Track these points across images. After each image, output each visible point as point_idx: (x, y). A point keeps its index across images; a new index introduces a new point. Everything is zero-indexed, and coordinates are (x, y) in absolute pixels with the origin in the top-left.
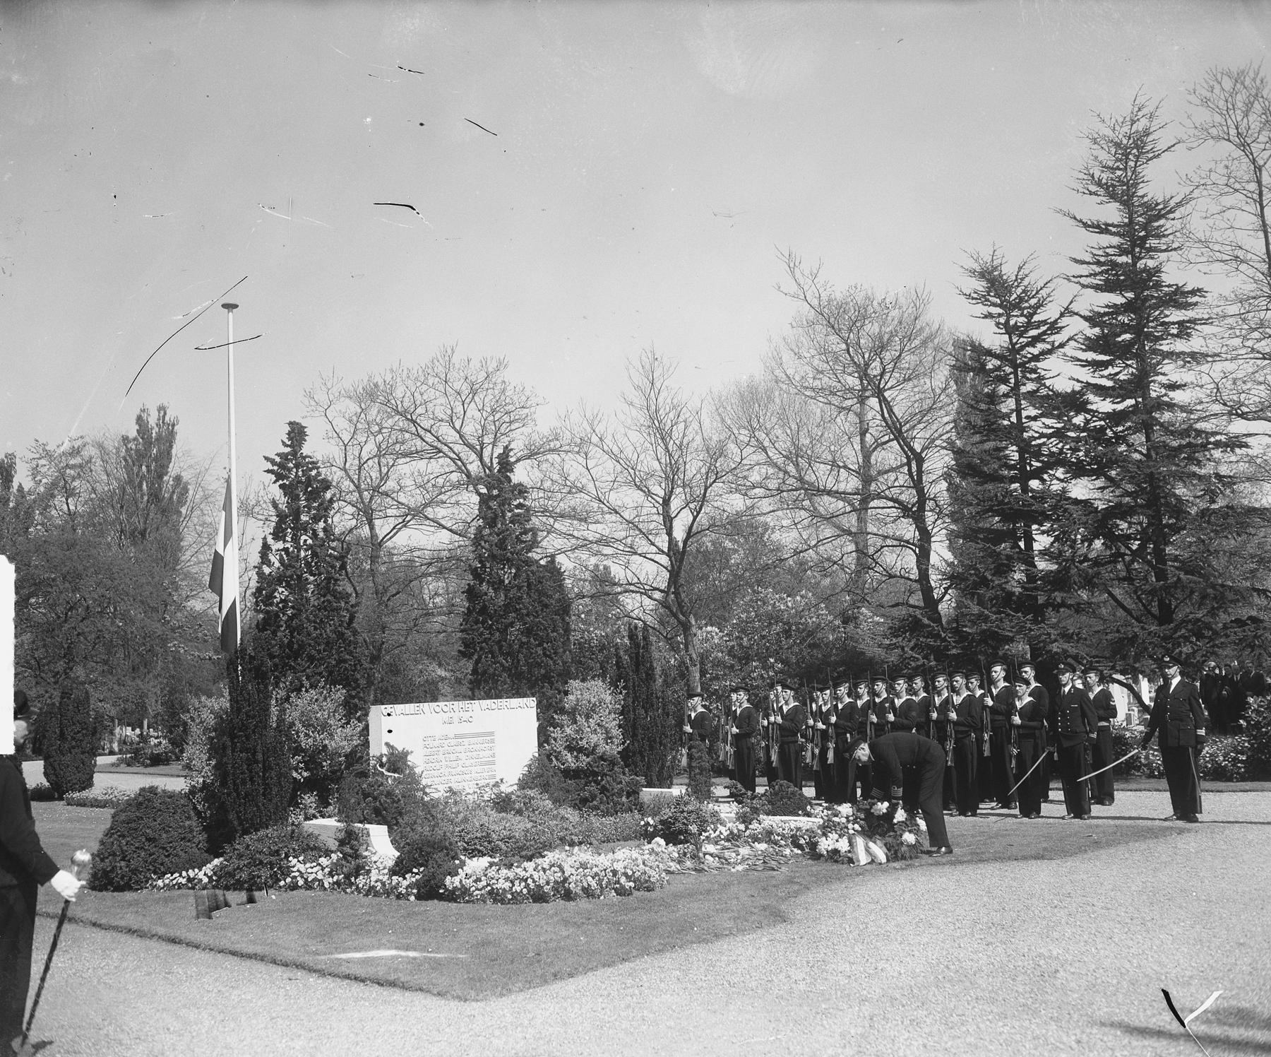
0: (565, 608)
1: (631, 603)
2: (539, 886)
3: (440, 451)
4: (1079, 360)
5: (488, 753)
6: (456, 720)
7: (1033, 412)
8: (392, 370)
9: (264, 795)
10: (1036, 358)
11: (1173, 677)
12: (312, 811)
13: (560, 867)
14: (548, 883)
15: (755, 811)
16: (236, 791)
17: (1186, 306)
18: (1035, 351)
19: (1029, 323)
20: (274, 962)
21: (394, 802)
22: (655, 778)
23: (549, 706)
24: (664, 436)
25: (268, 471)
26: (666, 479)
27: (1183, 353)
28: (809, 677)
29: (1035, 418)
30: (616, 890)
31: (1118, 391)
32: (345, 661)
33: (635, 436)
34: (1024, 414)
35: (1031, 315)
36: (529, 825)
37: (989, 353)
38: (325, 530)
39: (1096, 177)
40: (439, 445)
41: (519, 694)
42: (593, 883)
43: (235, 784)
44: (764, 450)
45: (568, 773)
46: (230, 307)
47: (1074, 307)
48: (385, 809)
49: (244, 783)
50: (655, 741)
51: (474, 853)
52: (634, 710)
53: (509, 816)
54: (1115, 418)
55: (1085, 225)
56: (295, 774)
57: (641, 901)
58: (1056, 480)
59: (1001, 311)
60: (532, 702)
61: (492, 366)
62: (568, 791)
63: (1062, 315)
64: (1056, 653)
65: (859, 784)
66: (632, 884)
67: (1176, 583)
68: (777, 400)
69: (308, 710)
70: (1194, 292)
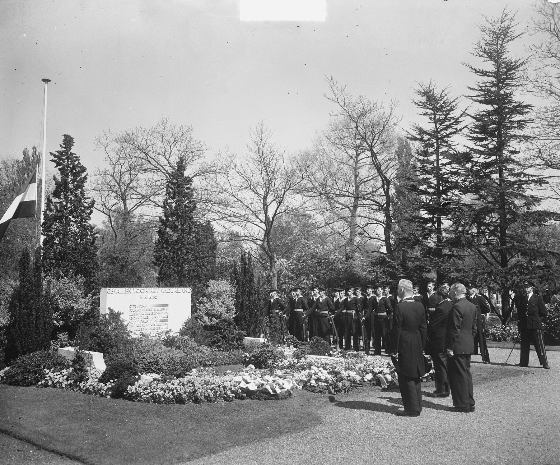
0: (214, 246)
1: (247, 246)
2: (180, 395)
3: (159, 169)
4: (470, 136)
5: (164, 315)
6: (148, 297)
7: (446, 161)
8: (137, 128)
9: (35, 332)
10: (447, 136)
11: (529, 292)
12: (64, 343)
13: (193, 384)
14: (185, 393)
15: (303, 352)
16: (20, 330)
17: (522, 113)
18: (448, 132)
19: (446, 118)
20: (15, 437)
21: (109, 339)
22: (251, 332)
23: (198, 292)
24: (266, 166)
25: (52, 161)
26: (266, 187)
27: (520, 136)
28: (331, 285)
29: (445, 165)
30: (224, 398)
31: (490, 152)
32: (88, 263)
33: (251, 165)
34: (440, 162)
35: (447, 114)
36: (183, 355)
37: (426, 133)
38: (81, 193)
39: (483, 47)
40: (159, 166)
41: (181, 285)
42: (211, 394)
43: (19, 327)
44: (312, 182)
45: (206, 327)
46: (46, 81)
47: (468, 112)
48: (103, 344)
49: (25, 326)
50: (252, 313)
51: (148, 371)
52: (242, 297)
53: (173, 350)
54: (486, 165)
55: (476, 71)
56: (55, 322)
57: (238, 405)
58: (454, 194)
59: (432, 112)
60: (189, 290)
61: (185, 129)
62: (206, 337)
63: (461, 115)
64: (453, 278)
65: (352, 337)
66: (233, 395)
67: (511, 247)
68: (319, 160)
69: (63, 290)
70: (526, 107)
